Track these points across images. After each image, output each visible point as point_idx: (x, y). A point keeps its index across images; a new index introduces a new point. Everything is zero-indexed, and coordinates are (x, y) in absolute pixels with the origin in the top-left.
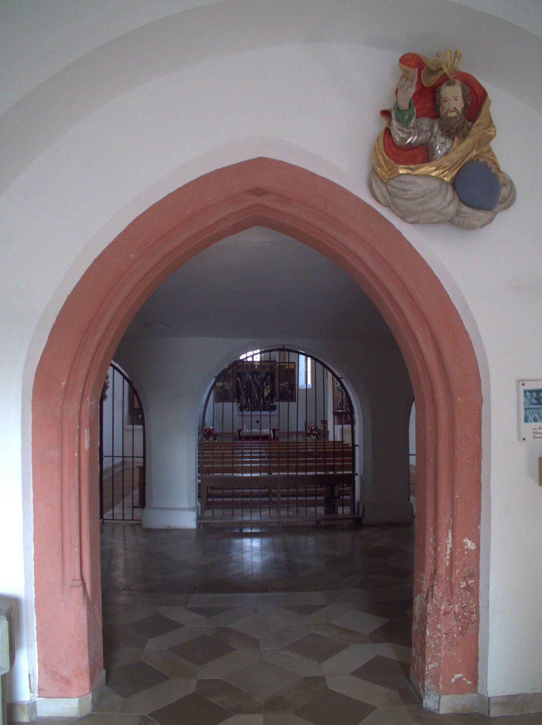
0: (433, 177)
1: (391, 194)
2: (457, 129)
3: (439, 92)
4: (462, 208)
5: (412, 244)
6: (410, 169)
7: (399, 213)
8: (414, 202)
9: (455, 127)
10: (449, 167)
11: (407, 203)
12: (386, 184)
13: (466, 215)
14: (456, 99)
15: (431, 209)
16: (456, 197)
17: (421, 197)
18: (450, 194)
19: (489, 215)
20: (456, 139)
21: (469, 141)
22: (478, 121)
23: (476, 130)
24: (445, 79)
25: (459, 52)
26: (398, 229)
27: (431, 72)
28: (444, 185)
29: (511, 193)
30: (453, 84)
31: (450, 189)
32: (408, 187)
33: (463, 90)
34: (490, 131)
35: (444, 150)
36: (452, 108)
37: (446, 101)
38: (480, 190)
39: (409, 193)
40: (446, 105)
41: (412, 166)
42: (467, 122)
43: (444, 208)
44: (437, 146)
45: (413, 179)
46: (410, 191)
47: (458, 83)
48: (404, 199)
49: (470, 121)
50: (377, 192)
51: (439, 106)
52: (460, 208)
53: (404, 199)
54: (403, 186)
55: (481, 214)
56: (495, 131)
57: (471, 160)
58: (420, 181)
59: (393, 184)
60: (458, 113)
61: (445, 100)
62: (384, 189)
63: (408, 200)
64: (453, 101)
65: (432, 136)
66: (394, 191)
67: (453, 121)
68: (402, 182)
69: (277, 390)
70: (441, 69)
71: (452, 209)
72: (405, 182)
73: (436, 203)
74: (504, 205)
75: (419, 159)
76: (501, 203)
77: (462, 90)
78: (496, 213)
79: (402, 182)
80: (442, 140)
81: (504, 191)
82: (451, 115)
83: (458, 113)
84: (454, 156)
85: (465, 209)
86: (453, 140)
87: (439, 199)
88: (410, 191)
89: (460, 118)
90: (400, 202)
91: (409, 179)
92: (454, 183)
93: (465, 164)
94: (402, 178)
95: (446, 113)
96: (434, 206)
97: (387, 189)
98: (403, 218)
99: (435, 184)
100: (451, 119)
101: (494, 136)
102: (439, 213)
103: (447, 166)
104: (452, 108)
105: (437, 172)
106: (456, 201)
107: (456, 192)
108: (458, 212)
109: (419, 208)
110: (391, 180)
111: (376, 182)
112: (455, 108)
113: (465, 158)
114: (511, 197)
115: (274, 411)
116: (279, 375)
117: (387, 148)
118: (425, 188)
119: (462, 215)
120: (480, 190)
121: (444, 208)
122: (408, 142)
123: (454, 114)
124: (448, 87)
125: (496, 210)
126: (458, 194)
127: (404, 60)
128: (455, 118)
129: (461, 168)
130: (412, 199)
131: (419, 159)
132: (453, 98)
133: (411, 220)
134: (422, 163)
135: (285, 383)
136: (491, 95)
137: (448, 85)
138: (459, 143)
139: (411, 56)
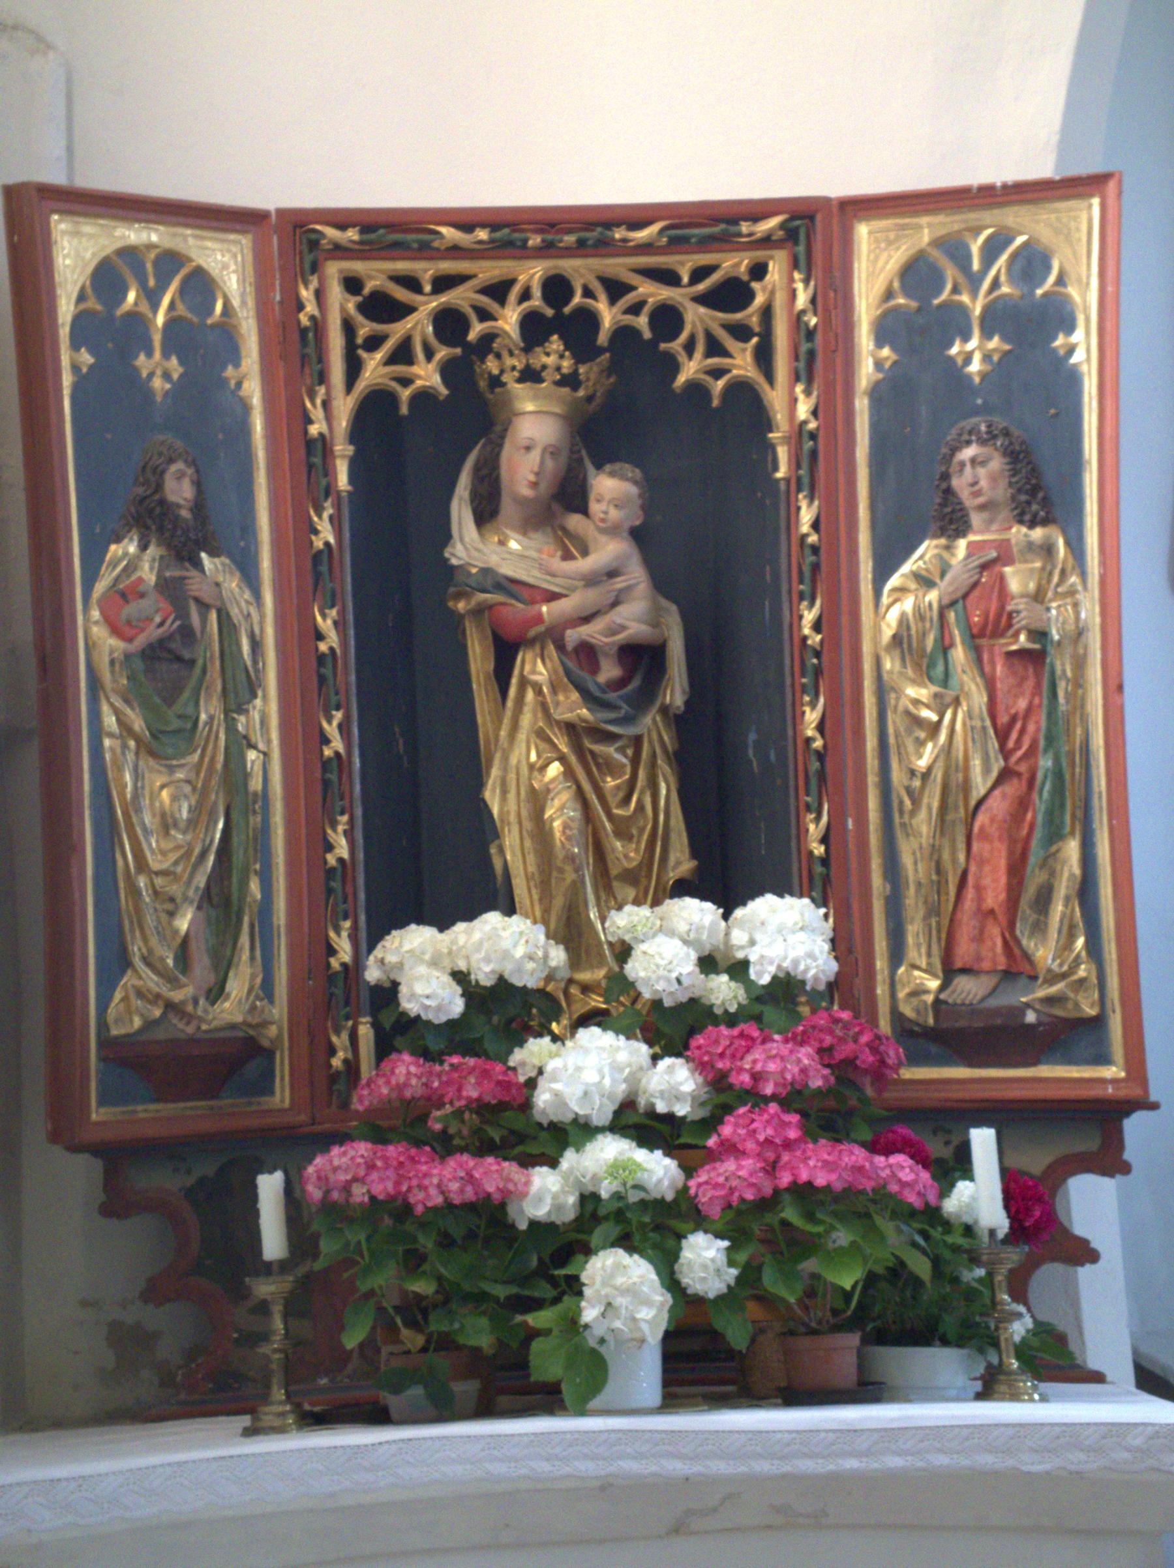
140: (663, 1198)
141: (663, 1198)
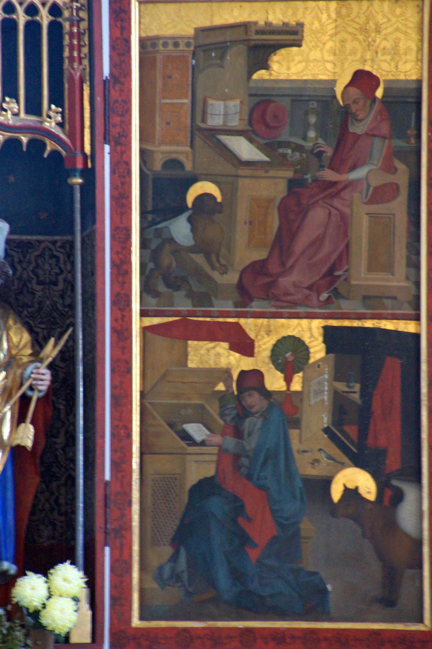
69: (124, 453)
115: (202, 31)
116: (165, 193)
135: (265, 332)
140: (357, 488)
141: (357, 488)
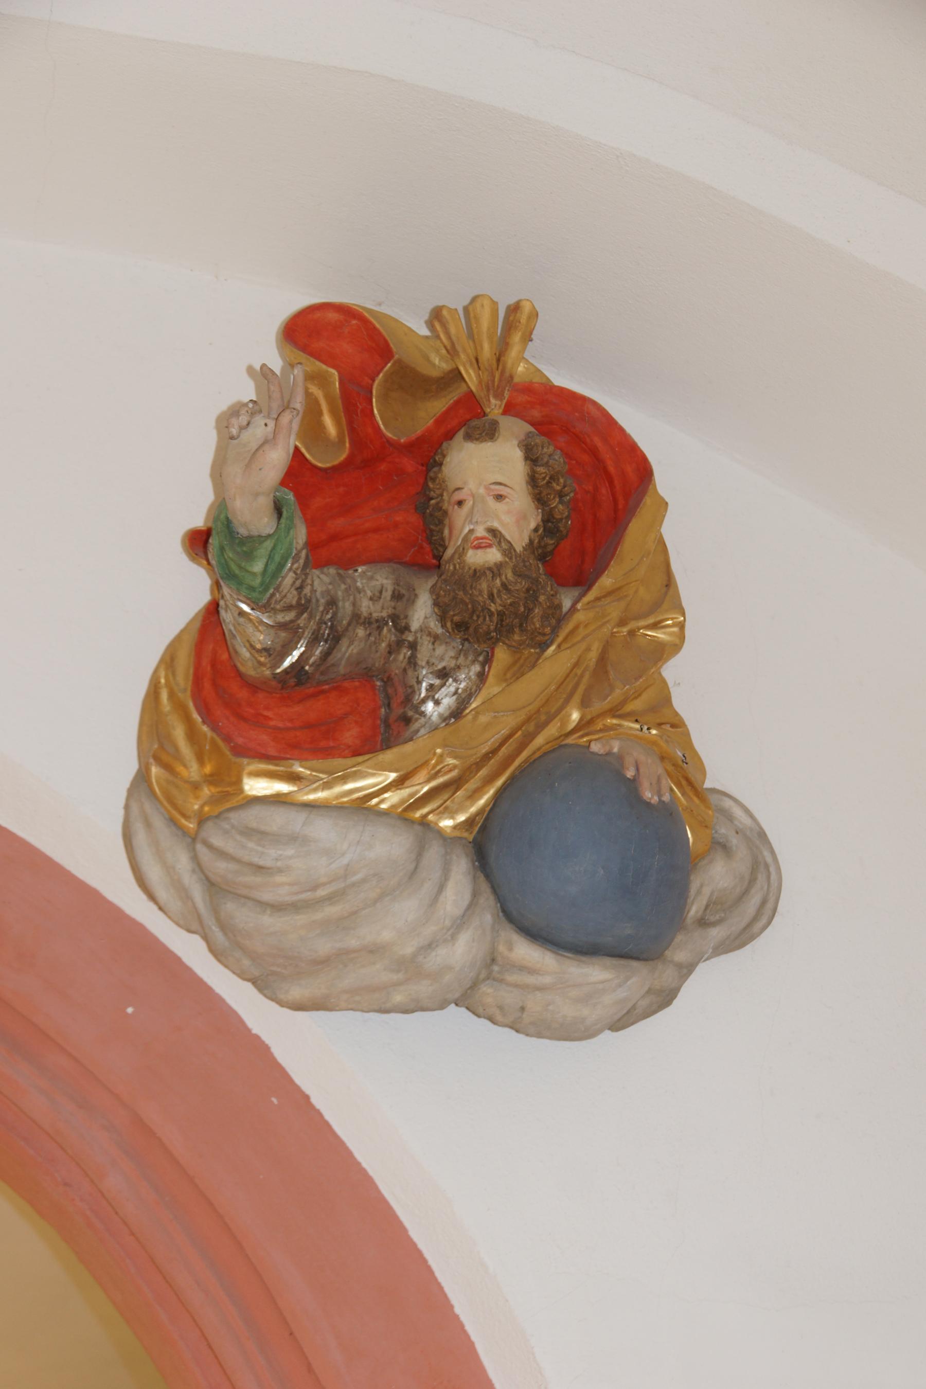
0: (385, 813)
1: (213, 886)
2: (501, 614)
3: (441, 464)
4: (511, 949)
5: (314, 1100)
6: (293, 778)
7: (246, 962)
8: (301, 919)
9: (493, 608)
10: (454, 773)
11: (268, 920)
12: (192, 839)
13: (531, 980)
14: (499, 497)
15: (374, 950)
16: (487, 900)
17: (330, 899)
18: (460, 884)
19: (632, 982)
20: (502, 655)
21: (555, 663)
22: (606, 581)
23: (588, 615)
24: (468, 419)
25: (526, 307)
26: (255, 1030)
27: (413, 383)
28: (434, 853)
29: (752, 881)
30: (490, 433)
31: (461, 867)
32: (270, 855)
33: (531, 457)
34: (655, 626)
35: (448, 702)
36: (480, 532)
37: (460, 503)
38: (613, 875)
39: (279, 879)
40: (459, 517)
41: (299, 769)
42: (549, 586)
43: (430, 946)
44: (419, 682)
45: (295, 821)
46: (280, 871)
47: (513, 430)
48: (264, 906)
49: (563, 582)
50: (154, 873)
51: (441, 522)
52: (502, 948)
53: (264, 906)
54: (252, 851)
55: (596, 973)
56: (682, 626)
57: (558, 747)
58: (323, 829)
59: (217, 841)
60: (509, 551)
61: (457, 496)
62: (183, 862)
63: (278, 908)
64: (491, 502)
65: (400, 643)
66: (220, 867)
67: (484, 586)
68: (248, 832)
70: (455, 376)
71: (461, 952)
72: (264, 834)
73: (398, 922)
74: (716, 934)
75: (350, 735)
76: (703, 923)
77: (527, 458)
78: (686, 970)
79: (248, 832)
80: (445, 655)
81: (715, 877)
82: (476, 558)
83: (509, 551)
84: (492, 722)
85: (525, 951)
86: (488, 660)
87: (407, 909)
88: (280, 871)
89: (518, 574)
90: (243, 916)
91: (277, 819)
92: (482, 844)
93: (531, 764)
94: (250, 817)
95: (461, 552)
96: (386, 936)
97: (195, 858)
98: (264, 984)
99: (388, 846)
100: (477, 574)
101: (676, 647)
102: (410, 968)
103: (455, 767)
104: (480, 532)
105: (404, 793)
106: (487, 915)
107: (488, 877)
108: (491, 966)
109: (324, 946)
110: (210, 824)
111: (148, 825)
112: (493, 532)
113: (530, 737)
114: (755, 900)
117: (207, 685)
118: (345, 860)
119: (512, 978)
120: (613, 875)
121: (430, 946)
122: (287, 663)
123: (493, 556)
124: (471, 446)
125: (680, 955)
126: (495, 890)
127: (306, 331)
128: (496, 570)
129: (512, 779)
130: (296, 907)
131: (350, 735)
132: (492, 491)
133: (296, 992)
134: (356, 753)
136: (664, 481)
137: (469, 437)
138: (516, 672)
139: (332, 316)
